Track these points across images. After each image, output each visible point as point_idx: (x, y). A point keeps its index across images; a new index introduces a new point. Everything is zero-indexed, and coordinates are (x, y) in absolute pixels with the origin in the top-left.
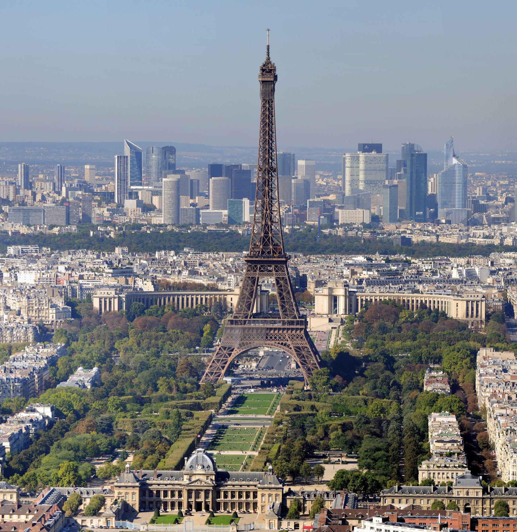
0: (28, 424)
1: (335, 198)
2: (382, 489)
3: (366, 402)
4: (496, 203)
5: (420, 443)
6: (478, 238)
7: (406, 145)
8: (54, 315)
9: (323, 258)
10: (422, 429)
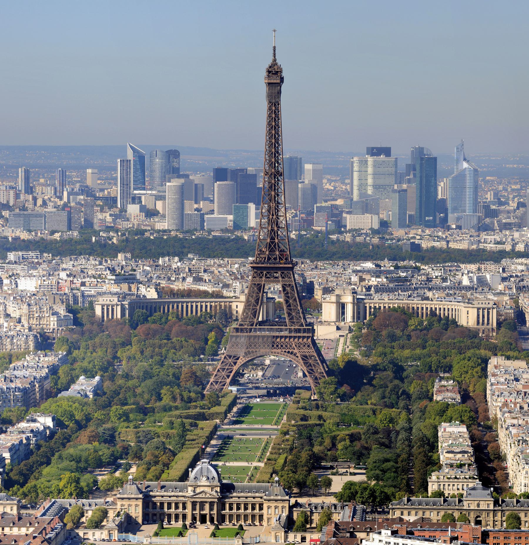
0: (29, 435)
1: (342, 203)
2: (391, 501)
3: (374, 412)
4: (508, 208)
5: (429, 454)
6: (489, 243)
7: (416, 148)
8: (56, 323)
9: (331, 264)
10: (431, 440)
